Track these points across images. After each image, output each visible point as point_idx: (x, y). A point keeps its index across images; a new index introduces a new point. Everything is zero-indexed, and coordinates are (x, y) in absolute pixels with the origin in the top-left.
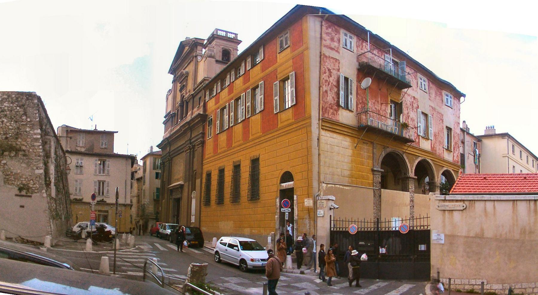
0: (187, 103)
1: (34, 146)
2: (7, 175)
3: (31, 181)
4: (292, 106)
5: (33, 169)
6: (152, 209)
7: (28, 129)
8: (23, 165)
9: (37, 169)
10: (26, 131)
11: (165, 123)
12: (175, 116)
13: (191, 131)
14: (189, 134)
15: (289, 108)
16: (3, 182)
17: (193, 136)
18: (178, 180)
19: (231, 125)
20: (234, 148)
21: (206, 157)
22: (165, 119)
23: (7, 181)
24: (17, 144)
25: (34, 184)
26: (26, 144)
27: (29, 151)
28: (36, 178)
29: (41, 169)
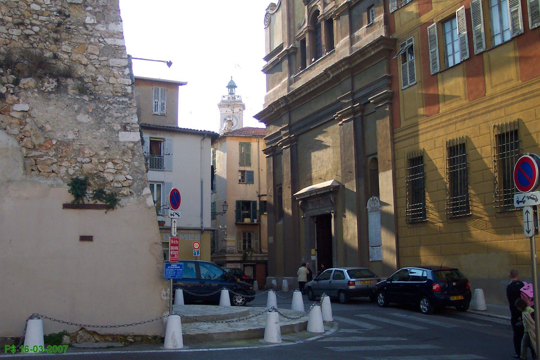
0: (329, 23)
1: (108, 66)
2: (34, 148)
3: (110, 165)
4: (513, 39)
5: (112, 130)
6: (233, 244)
7: (89, 20)
8: (83, 118)
9: (124, 129)
10: (85, 25)
11: (267, 70)
12: (295, 53)
13: (353, 77)
14: (347, 83)
15: (504, 43)
16: (21, 170)
17: (358, 86)
18: (322, 179)
19: (477, 51)
20: (492, 98)
21: (403, 124)
22: (265, 63)
23: (32, 166)
24: (55, 57)
25: (118, 172)
26: (85, 61)
27: (94, 79)
28: (124, 153)
29: (133, 130)
